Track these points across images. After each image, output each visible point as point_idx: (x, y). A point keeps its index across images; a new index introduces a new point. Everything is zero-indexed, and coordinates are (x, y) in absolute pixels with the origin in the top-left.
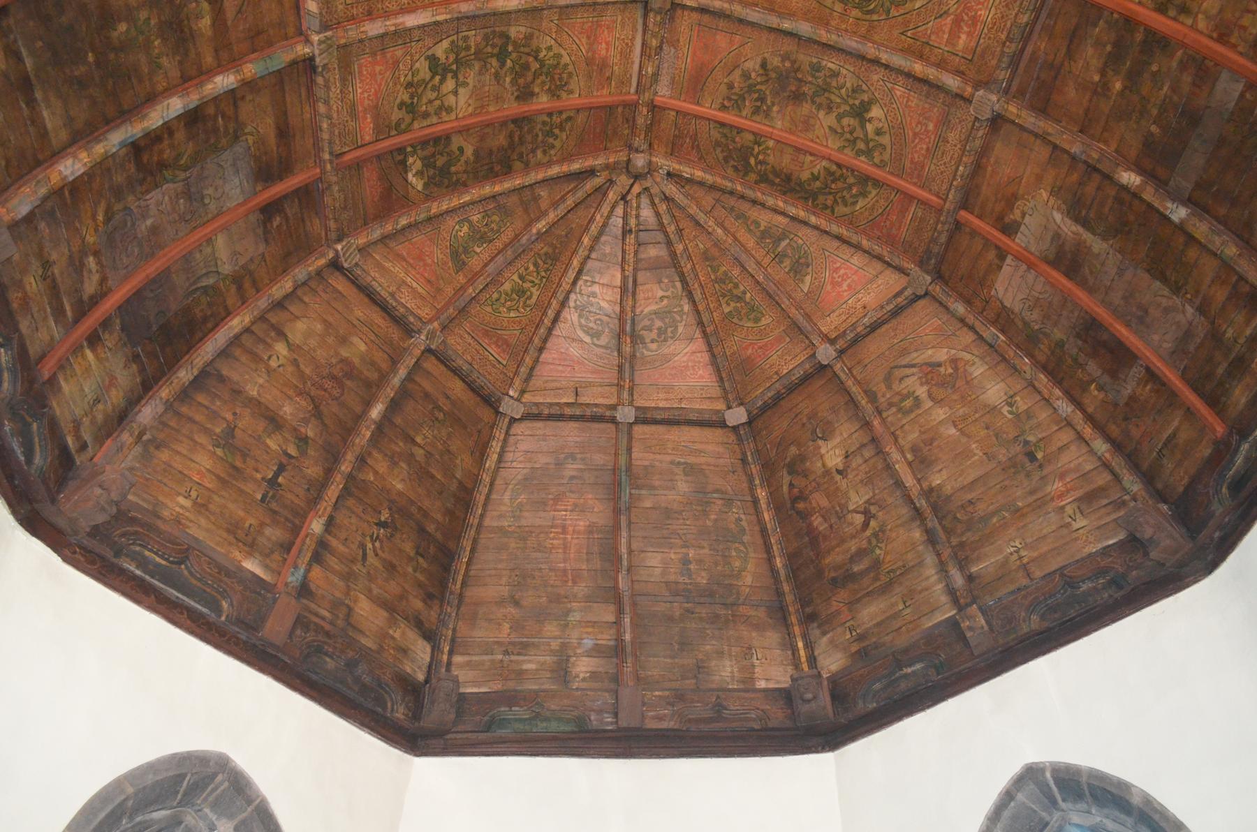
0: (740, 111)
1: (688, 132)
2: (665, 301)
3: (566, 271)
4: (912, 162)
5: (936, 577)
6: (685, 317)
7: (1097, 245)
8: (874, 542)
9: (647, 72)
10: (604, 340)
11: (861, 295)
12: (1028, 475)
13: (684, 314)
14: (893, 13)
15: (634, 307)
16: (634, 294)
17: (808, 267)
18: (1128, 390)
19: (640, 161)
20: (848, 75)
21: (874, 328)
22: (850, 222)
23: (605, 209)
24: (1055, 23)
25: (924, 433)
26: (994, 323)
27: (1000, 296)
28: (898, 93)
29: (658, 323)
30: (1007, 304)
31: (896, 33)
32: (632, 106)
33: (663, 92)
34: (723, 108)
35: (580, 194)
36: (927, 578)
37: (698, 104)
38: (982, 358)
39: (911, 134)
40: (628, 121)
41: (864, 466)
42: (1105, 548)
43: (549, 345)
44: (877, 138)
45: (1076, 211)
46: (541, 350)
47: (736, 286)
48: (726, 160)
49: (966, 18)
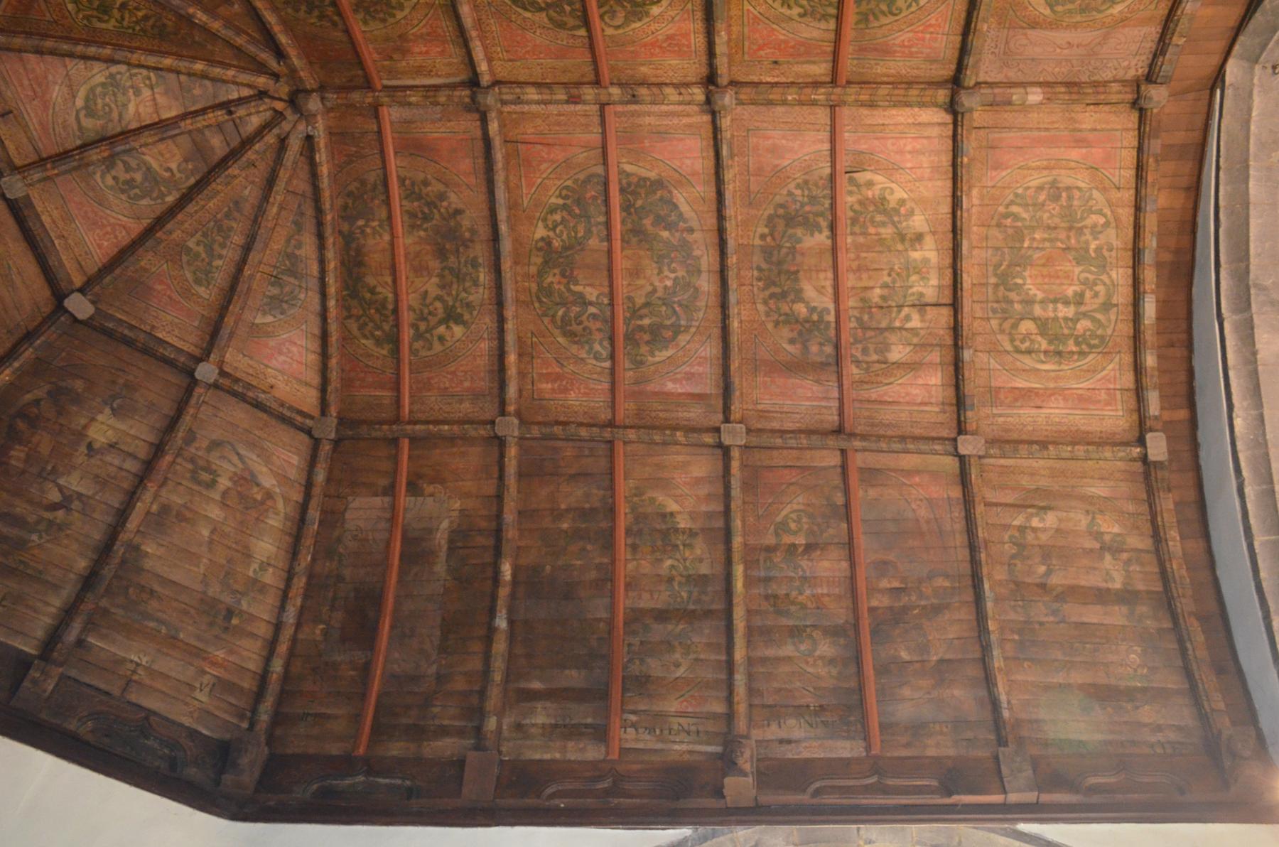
0: (406, 198)
1: (363, 148)
2: (167, 175)
3: (152, 52)
4: (429, 379)
5: (53, 610)
6: (159, 201)
7: (440, 568)
8: (41, 527)
9: (410, 96)
10: (88, 123)
11: (280, 378)
12: (211, 624)
13: (163, 199)
14: (546, 320)
15: (146, 145)
16: (162, 140)
17: (282, 314)
18: (338, 658)
19: (314, 104)
20: (481, 294)
21: (258, 405)
22: (346, 338)
23: (245, 78)
24: (587, 456)
25: (187, 508)
26: (323, 512)
27: (351, 506)
28: (482, 345)
29: (138, 177)
30: (347, 516)
31: (531, 327)
32: (368, 85)
33: (392, 114)
34: (402, 181)
35: (252, 49)
36: (47, 604)
37: (396, 153)
38: (287, 518)
39: (453, 369)
40: (350, 81)
41: (115, 469)
42: (196, 731)
43: (49, 58)
44: (435, 338)
45: (459, 537)
46: (39, 52)
47: (223, 246)
48: (350, 194)
49: (564, 383)
